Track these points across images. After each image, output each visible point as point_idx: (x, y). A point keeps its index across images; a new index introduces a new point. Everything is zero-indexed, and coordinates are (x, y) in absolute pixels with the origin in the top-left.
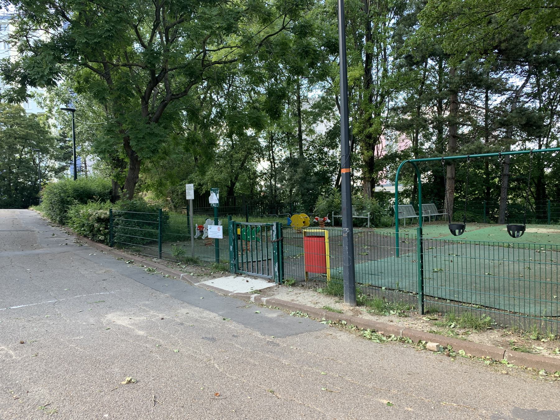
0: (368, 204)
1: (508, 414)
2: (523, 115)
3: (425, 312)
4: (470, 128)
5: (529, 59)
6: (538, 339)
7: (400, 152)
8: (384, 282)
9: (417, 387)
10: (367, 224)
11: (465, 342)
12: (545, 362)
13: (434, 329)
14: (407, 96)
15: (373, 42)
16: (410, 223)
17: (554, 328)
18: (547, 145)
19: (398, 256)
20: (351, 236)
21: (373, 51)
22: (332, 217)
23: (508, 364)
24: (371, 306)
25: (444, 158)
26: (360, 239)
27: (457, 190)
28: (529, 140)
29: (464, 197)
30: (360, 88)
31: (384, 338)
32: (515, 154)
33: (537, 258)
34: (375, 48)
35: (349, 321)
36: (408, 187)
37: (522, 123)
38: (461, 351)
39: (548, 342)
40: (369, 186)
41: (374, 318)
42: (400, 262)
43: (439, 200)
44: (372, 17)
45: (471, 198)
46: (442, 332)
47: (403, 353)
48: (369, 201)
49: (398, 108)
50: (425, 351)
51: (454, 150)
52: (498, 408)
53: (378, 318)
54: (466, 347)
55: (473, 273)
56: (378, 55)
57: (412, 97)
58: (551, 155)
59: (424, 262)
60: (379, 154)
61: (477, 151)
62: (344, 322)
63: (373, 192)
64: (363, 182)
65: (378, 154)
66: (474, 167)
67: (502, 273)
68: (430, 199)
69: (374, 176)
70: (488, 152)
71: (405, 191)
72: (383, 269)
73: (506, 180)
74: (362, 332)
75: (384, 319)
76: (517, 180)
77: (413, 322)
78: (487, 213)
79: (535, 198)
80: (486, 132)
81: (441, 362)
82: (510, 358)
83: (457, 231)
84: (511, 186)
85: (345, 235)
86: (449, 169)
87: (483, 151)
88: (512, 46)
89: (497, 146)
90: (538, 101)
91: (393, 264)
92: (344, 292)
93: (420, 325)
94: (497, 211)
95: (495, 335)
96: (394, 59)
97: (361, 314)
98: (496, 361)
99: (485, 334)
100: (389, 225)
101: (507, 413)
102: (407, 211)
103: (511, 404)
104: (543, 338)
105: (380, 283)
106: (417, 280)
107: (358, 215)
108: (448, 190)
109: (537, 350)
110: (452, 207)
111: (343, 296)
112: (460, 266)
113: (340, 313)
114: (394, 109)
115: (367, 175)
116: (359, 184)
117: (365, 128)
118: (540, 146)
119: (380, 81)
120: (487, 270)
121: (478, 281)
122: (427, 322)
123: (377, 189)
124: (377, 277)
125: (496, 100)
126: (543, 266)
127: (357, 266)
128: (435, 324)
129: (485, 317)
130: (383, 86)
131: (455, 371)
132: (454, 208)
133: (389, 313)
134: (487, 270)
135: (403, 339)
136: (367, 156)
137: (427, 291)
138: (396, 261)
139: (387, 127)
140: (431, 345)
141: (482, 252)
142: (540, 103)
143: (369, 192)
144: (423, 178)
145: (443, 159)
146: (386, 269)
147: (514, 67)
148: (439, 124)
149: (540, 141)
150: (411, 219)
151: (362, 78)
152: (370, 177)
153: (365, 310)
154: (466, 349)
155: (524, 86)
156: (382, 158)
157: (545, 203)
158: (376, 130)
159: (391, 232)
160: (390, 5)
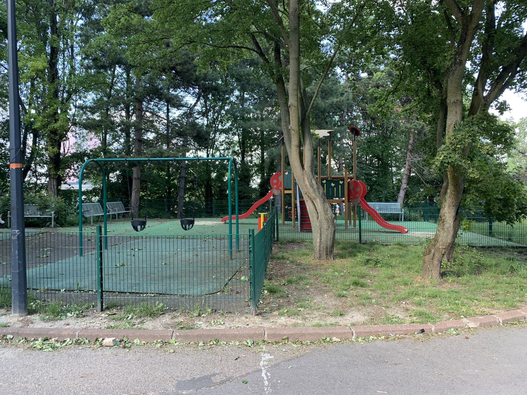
0: (52, 203)
1: (172, 389)
2: (194, 128)
3: (104, 308)
4: (154, 135)
5: (198, 84)
6: (199, 315)
7: (89, 152)
8: (62, 284)
9: (90, 388)
10: (51, 224)
11: (140, 331)
12: (203, 335)
13: (112, 324)
14: (97, 97)
15: (58, 36)
16: (97, 221)
17: (211, 304)
18: (213, 155)
19: (81, 255)
20: (22, 238)
21: (59, 46)
22: (7, 218)
23: (176, 342)
24: (45, 312)
25: (127, 159)
26: (41, 240)
27: (143, 189)
28: (200, 150)
29: (149, 195)
30: (44, 80)
31: (58, 345)
32: (189, 160)
33: (203, 246)
34: (61, 43)
35: (16, 334)
36: (97, 186)
37: (194, 135)
38: (136, 340)
39: (206, 316)
40: (55, 183)
41: (47, 325)
42: (82, 261)
43: (126, 198)
44: (57, 10)
45: (156, 196)
46: (119, 325)
47: (77, 356)
48: (53, 199)
49: (86, 107)
50: (101, 348)
51: (139, 153)
52: (164, 386)
53: (52, 324)
54: (140, 335)
55: (152, 265)
56: (64, 51)
57: (101, 99)
58: (215, 163)
59: (103, 260)
60: (66, 151)
61: (159, 155)
62: (9, 337)
63: (59, 190)
64: (48, 179)
65: (64, 151)
66: (157, 169)
67: (176, 261)
68: (118, 197)
69: (60, 173)
70: (168, 157)
71: (94, 189)
72: (64, 270)
73: (183, 181)
74: (32, 343)
75: (60, 324)
76: (192, 182)
77: (92, 321)
78: (169, 209)
79: (204, 197)
80: (167, 139)
81: (116, 355)
82: (177, 337)
83: (139, 227)
84: (188, 186)
85: (14, 238)
86: (134, 169)
87: (164, 155)
88: (185, 70)
89: (175, 152)
90: (205, 119)
91: (75, 264)
92: (13, 302)
93: (98, 322)
94: (177, 207)
95: (166, 319)
96: (82, 59)
97: (32, 323)
98: (166, 343)
99: (158, 320)
100: (75, 224)
101: (171, 388)
102: (94, 209)
103: (176, 379)
104: (203, 313)
105: (57, 285)
106: (97, 277)
107: (40, 215)
108: (135, 189)
109: (198, 325)
110: (138, 205)
111: (11, 306)
112: (141, 259)
113: (5, 326)
114: (81, 107)
115: (52, 173)
116: (43, 181)
117: (49, 123)
118: (208, 156)
119: (67, 78)
120: (164, 261)
121: (156, 272)
122: (105, 318)
123: (64, 187)
124: (53, 279)
125: (175, 113)
126: (207, 253)
127: (30, 272)
128: (113, 319)
129: (158, 304)
130: (69, 83)
131: (129, 361)
132: (139, 205)
133: (66, 316)
134: (164, 261)
135: (79, 341)
136: (52, 152)
137: (106, 287)
138: (79, 261)
139: (75, 124)
140: (108, 341)
141: (160, 245)
142: (207, 121)
143: (54, 189)
144: (112, 178)
145: (126, 161)
146: (68, 269)
147: (188, 88)
148: (126, 128)
149: (208, 151)
150: (98, 217)
151: (47, 71)
152: (56, 175)
153: (38, 318)
154: (140, 337)
155: (195, 105)
156: (69, 156)
157: (211, 201)
158: (63, 127)
159: (75, 230)
160: (77, 5)
